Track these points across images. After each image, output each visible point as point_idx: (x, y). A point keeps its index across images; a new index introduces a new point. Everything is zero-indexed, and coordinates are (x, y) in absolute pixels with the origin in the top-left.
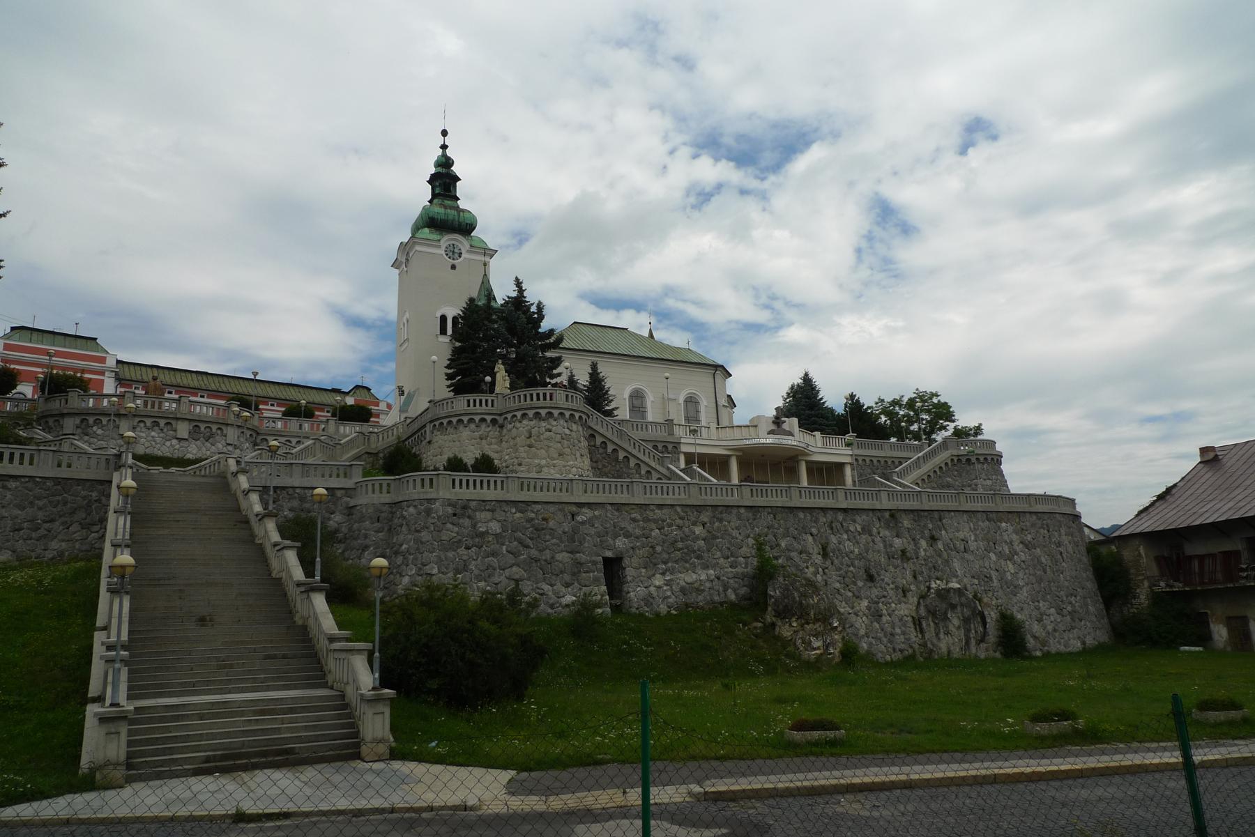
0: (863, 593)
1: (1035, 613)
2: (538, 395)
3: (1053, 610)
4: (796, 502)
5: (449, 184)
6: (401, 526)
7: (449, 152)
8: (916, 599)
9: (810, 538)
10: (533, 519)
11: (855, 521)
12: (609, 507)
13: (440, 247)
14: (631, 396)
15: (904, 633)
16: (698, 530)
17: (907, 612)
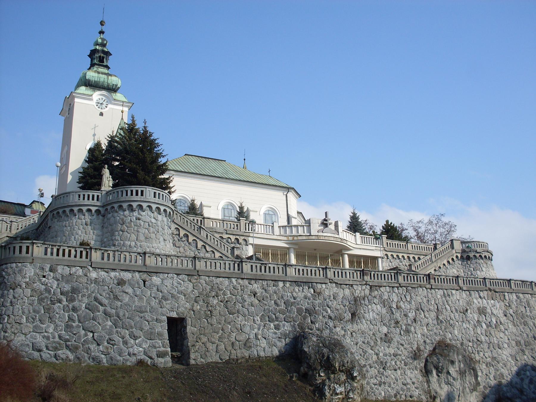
2: (137, 191)
14: (224, 209)
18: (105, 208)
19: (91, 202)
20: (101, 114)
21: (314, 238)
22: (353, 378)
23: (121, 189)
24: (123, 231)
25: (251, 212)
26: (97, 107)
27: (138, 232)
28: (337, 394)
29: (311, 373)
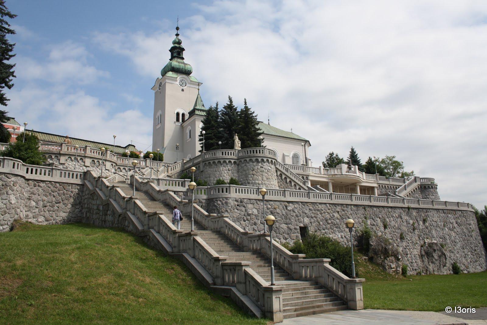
0: (400, 245)
1: (463, 254)
3: (469, 253)
4: (355, 202)
5: (180, 52)
8: (420, 247)
9: (379, 219)
10: (270, 208)
12: (300, 204)
15: (416, 262)
16: (336, 215)
17: (417, 253)
19: (230, 157)
21: (344, 176)
22: (398, 260)
23: (250, 149)
25: (286, 157)
26: (180, 86)
27: (262, 175)
28: (392, 268)
29: (376, 257)
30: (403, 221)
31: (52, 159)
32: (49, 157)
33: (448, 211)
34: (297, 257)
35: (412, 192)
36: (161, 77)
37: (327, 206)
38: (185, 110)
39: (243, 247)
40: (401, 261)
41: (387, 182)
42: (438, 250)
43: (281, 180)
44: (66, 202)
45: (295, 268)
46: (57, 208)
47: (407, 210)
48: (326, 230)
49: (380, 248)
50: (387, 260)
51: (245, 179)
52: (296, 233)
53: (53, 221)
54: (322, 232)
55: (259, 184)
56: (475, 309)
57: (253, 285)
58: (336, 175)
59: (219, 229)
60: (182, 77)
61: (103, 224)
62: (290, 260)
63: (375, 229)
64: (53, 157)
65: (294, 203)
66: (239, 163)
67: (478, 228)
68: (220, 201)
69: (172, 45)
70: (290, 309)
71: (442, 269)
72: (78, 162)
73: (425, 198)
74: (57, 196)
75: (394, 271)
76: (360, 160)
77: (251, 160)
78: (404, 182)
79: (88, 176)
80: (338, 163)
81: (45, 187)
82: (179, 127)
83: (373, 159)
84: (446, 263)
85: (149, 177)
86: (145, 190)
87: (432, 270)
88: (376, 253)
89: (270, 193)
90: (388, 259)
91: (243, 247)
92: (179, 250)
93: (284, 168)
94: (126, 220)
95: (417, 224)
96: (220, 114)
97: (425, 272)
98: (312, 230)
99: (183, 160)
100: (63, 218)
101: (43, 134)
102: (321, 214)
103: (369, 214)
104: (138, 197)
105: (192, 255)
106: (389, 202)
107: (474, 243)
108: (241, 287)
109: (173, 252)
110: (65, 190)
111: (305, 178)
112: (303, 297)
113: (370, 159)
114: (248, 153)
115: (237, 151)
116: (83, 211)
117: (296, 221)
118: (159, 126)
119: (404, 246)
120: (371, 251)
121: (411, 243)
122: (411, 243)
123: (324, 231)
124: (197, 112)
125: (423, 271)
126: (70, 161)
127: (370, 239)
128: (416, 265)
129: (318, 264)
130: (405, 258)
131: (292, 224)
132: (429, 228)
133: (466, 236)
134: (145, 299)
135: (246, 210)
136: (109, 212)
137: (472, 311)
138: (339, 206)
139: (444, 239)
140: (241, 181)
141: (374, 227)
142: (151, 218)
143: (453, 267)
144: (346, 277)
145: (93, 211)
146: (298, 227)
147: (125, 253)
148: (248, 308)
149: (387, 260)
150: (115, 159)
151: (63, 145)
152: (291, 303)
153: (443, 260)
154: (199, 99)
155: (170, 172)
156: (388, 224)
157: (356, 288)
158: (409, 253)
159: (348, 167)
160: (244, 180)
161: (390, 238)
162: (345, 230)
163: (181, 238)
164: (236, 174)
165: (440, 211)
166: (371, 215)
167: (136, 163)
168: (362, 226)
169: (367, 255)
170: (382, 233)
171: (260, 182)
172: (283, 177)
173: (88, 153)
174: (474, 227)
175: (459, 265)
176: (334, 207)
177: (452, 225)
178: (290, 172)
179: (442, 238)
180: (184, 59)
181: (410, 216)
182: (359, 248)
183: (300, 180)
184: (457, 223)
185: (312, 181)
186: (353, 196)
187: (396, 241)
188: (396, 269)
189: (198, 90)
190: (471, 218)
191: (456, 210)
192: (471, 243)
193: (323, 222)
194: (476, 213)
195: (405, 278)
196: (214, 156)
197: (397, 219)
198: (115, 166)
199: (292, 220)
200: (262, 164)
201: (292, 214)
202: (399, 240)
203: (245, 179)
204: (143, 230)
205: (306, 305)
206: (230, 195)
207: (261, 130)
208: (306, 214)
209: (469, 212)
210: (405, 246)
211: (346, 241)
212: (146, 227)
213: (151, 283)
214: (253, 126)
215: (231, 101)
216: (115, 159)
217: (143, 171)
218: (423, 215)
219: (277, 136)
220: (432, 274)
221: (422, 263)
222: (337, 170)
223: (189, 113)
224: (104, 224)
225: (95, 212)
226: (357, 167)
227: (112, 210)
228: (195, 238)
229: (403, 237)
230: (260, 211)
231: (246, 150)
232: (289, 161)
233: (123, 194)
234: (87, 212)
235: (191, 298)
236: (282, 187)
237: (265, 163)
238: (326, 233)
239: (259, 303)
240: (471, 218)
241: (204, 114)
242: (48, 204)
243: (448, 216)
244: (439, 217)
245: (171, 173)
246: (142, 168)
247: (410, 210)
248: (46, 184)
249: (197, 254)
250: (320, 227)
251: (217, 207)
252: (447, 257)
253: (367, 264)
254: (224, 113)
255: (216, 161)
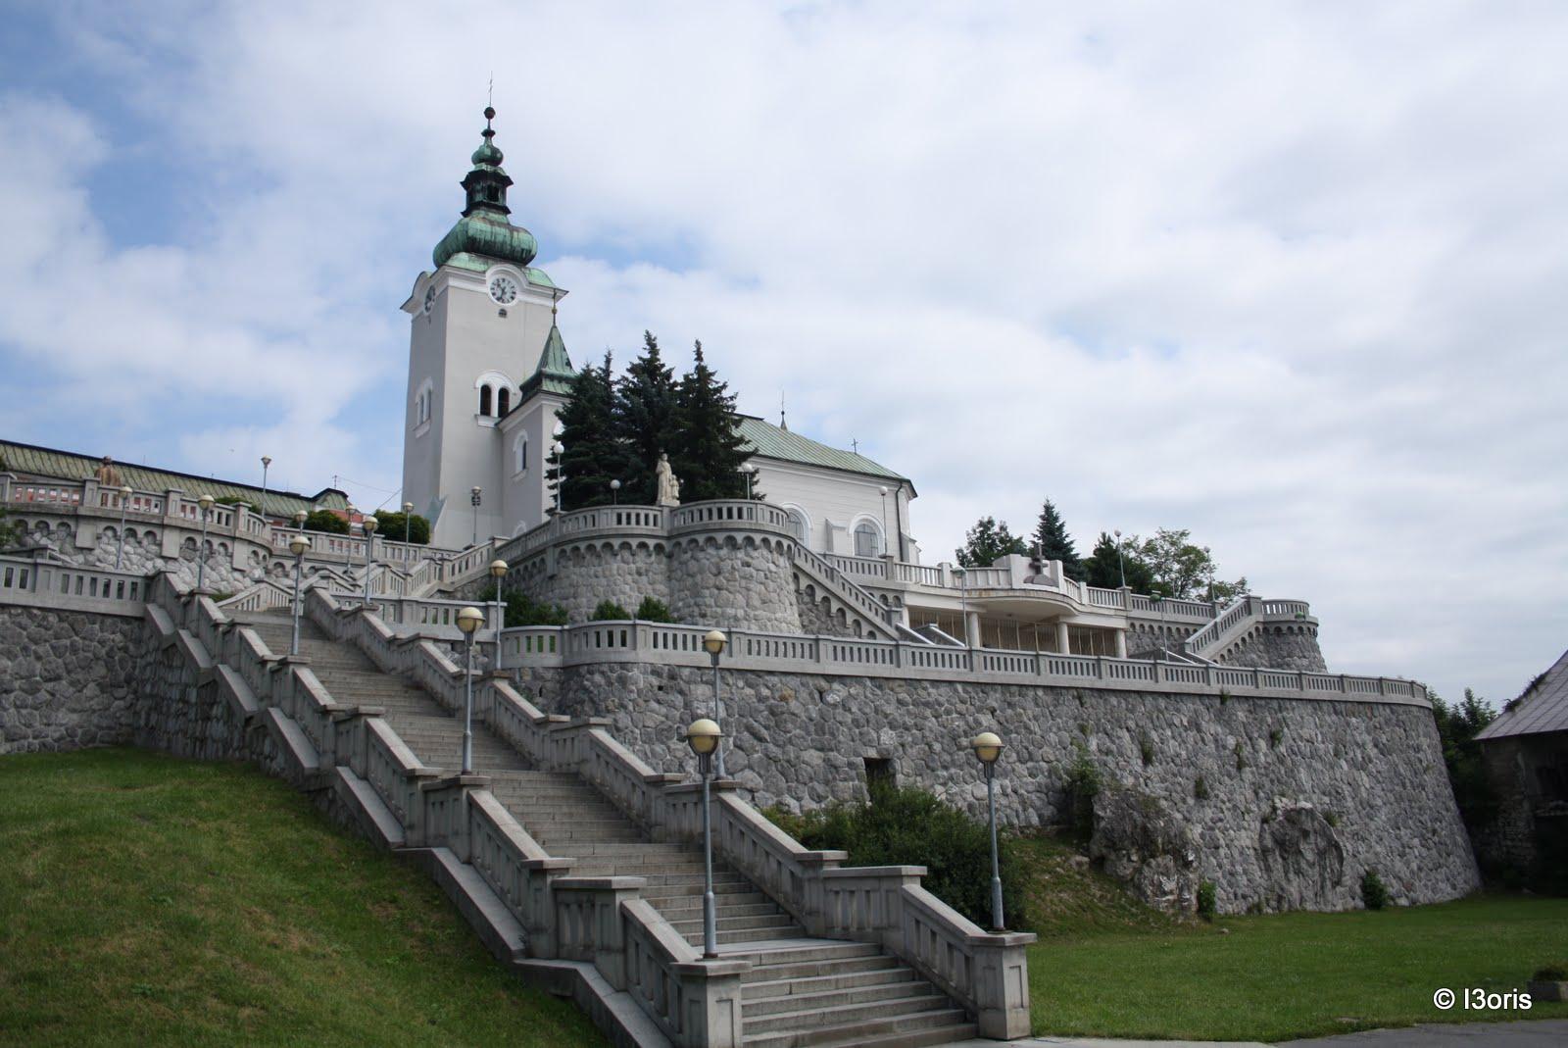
0: (1195, 816)
1: (1396, 845)
2: (730, 511)
3: (1416, 841)
4: (1109, 682)
5: (496, 190)
6: (582, 702)
7: (495, 142)
8: (1258, 824)
9: (1127, 734)
10: (767, 698)
11: (1178, 710)
12: (868, 683)
13: (483, 282)
15: (1245, 872)
17: (1248, 842)
18: (674, 541)
19: (642, 529)
20: (503, 313)
21: (1017, 594)
22: (1187, 864)
24: (719, 589)
25: (834, 531)
26: (493, 299)
27: (748, 589)
28: (1165, 893)
29: (1113, 856)
30: (1203, 740)
31: (49, 534)
32: (37, 526)
33: (1349, 705)
34: (819, 862)
35: (1236, 645)
36: (431, 268)
37: (956, 690)
38: (508, 378)
39: (651, 826)
40: (1196, 869)
41: (1153, 612)
42: (1315, 832)
43: (810, 606)
44: (80, 676)
45: (813, 897)
46: (48, 697)
47: (1218, 702)
48: (953, 771)
49: (1129, 829)
50: (1149, 865)
51: (692, 602)
52: (853, 780)
53: (30, 740)
54: (938, 776)
55: (736, 619)
56: (1529, 997)
57: (649, 957)
58: (992, 589)
59: (574, 768)
60: (497, 272)
61: (197, 750)
62: (798, 870)
63: (1112, 765)
64: (53, 524)
65: (848, 681)
66: (674, 547)
67: (1443, 761)
68: (603, 673)
69: (472, 168)
70: (776, 1039)
71: (1330, 895)
72: (140, 543)
73: (1279, 666)
74: (48, 655)
75: (1172, 904)
76: (1072, 542)
77: (710, 540)
78: (1214, 615)
79: (160, 590)
80: (1008, 551)
81: (9, 624)
82: (488, 433)
83: (1116, 542)
84: (1341, 874)
85: (363, 596)
86: (349, 637)
87: (1296, 896)
88: (1114, 844)
89: (768, 646)
90: (1153, 862)
91: (651, 827)
92: (426, 837)
93: (823, 568)
94: (265, 736)
95: (1249, 748)
96: (619, 391)
97: (1273, 903)
98: (905, 770)
99: (494, 539)
100: (67, 730)
101: (36, 454)
102: (936, 717)
103: (1093, 717)
104: (308, 659)
105: (464, 854)
106: (1160, 679)
107: (1431, 809)
108: (613, 963)
109: (405, 845)
110: (77, 635)
111: (891, 599)
112: (828, 997)
113: (1107, 541)
114: (701, 519)
115: (666, 511)
116: (138, 707)
117: (853, 740)
118: (426, 428)
119: (1207, 820)
120: (1097, 836)
121: (1228, 809)
122: (1228, 809)
123: (945, 773)
124: (547, 385)
125: (1267, 900)
126: (112, 541)
127: (1096, 798)
128: (1246, 883)
129: (886, 885)
130: (1212, 858)
131: (838, 751)
132: (1288, 761)
133: (1404, 786)
134: (263, 1008)
135: (687, 705)
136: (216, 711)
137: (1519, 1002)
138: (996, 691)
139: (1338, 795)
140: (678, 610)
141: (1109, 759)
142: (342, 728)
143: (1364, 888)
144: (973, 930)
145: (169, 707)
146: (860, 761)
147: (238, 849)
148: (628, 1035)
149: (1149, 865)
150: (265, 534)
151: (89, 485)
152: (783, 1019)
153: (1331, 865)
154: (555, 343)
155: (448, 579)
156: (1156, 748)
157: (1006, 965)
158: (1222, 842)
159: (1031, 566)
160: (689, 606)
161: (1163, 793)
162: (1014, 770)
163: (432, 797)
164: (662, 588)
165: (1325, 706)
166: (1099, 720)
167: (303, 545)
168: (1071, 756)
169: (1086, 852)
170: (1136, 778)
171: (740, 613)
172: (819, 595)
173: (175, 513)
174: (1430, 757)
175: (1383, 880)
176: (981, 694)
177: (1363, 753)
178: (841, 581)
179: (1330, 794)
180: (509, 212)
181: (1227, 724)
182: (1061, 826)
183: (874, 606)
184: (1376, 746)
185: (912, 610)
186: (1159, 667)
187: (1180, 804)
188: (1180, 895)
189: (554, 311)
190: (1421, 729)
191: (1380, 703)
192: (1420, 809)
193: (942, 743)
194: (1438, 712)
195: (1208, 926)
196: (590, 527)
197: (1184, 734)
198: (264, 557)
199: (841, 738)
200: (747, 555)
201: (839, 718)
202: (1191, 801)
203: (692, 602)
204: (318, 769)
205: (832, 1023)
206: (633, 653)
207: (747, 442)
208: (886, 716)
209: (1414, 709)
210: (1212, 820)
211: (1017, 806)
212: (327, 761)
213: (305, 952)
214: (725, 431)
215: (653, 349)
216: (265, 534)
217: (359, 573)
218: (1269, 720)
219: (806, 464)
220: (1297, 910)
221: (1265, 876)
222: (995, 573)
223: (522, 388)
224: (201, 749)
225: (173, 710)
226: (1060, 564)
227: (224, 702)
228: (475, 796)
229: (1206, 792)
230: (735, 706)
231: (695, 507)
232: (845, 546)
233: (262, 649)
234: (150, 709)
235: (438, 1001)
236: (815, 628)
237: (756, 549)
238: (951, 778)
239: (666, 1019)
240: (1421, 729)
241: (565, 388)
242: (17, 684)
243: (1348, 724)
244: (1322, 726)
245: (453, 583)
246: (354, 565)
247: (1228, 703)
248: (10, 615)
249: (477, 851)
250: (933, 760)
251: (591, 692)
252: (1345, 855)
253: (1086, 880)
254: (630, 389)
255: (598, 544)
